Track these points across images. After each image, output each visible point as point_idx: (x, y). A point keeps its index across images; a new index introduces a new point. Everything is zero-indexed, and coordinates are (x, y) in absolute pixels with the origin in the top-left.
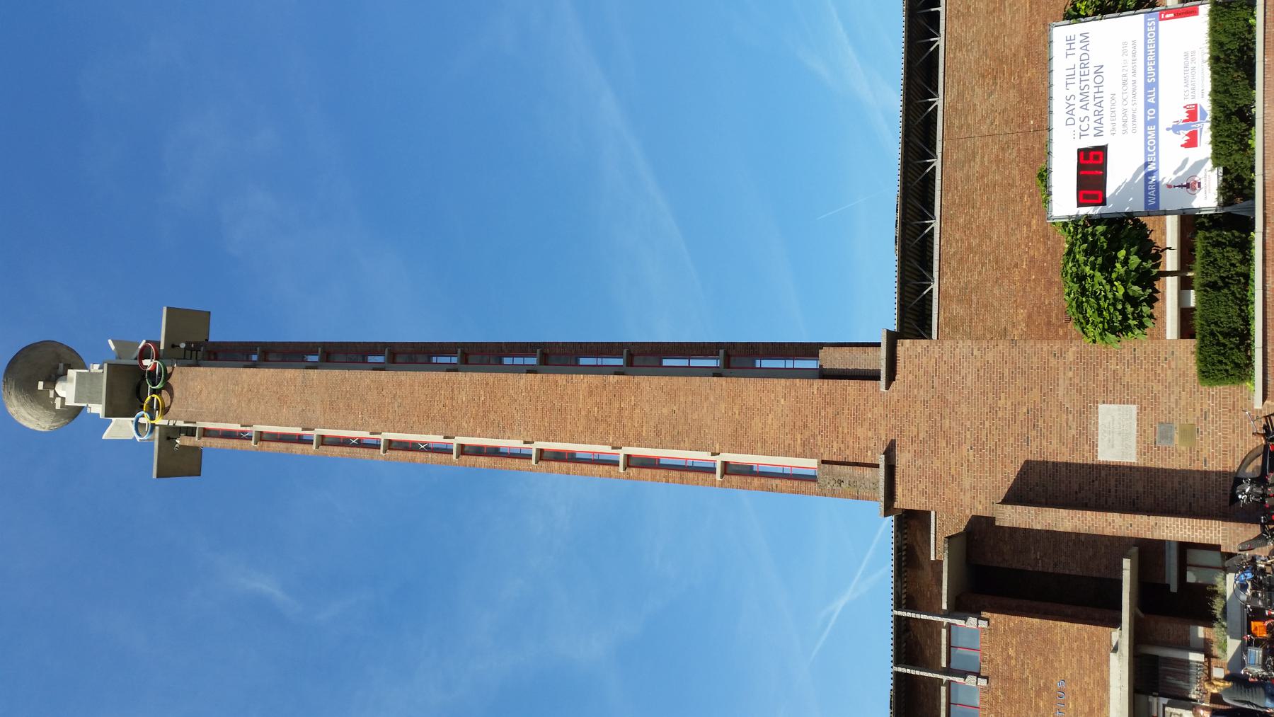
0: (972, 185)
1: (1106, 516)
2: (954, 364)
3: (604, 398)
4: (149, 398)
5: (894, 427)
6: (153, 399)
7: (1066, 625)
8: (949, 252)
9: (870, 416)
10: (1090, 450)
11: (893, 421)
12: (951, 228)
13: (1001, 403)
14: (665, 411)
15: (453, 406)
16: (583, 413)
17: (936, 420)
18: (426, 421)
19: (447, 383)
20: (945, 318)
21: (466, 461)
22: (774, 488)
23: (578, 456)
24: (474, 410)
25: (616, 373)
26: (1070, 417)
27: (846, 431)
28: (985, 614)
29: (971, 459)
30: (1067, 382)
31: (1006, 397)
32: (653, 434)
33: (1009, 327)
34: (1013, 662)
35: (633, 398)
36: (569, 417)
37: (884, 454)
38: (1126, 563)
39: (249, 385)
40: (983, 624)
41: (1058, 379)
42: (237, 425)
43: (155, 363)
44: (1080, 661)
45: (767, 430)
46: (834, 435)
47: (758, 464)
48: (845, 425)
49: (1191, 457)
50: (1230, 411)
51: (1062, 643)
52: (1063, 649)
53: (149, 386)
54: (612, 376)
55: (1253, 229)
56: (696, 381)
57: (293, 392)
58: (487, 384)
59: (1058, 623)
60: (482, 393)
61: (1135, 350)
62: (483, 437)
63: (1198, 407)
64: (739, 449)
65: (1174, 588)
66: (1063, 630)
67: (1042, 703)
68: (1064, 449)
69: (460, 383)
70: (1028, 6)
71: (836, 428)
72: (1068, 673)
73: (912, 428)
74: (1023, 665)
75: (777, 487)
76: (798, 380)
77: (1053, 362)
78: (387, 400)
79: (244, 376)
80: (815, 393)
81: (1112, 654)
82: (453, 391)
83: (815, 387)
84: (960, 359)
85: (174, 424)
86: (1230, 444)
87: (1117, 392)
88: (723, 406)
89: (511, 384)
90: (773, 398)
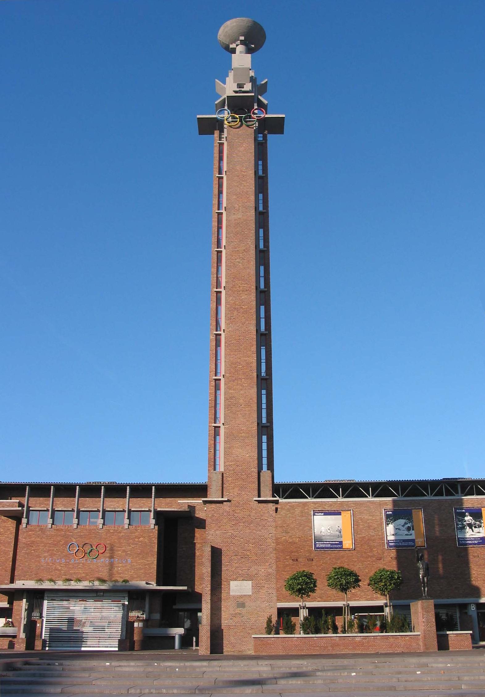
0: (358, 515)
1: (209, 585)
2: (266, 527)
3: (246, 371)
4: (237, 116)
5: (239, 503)
6: (237, 119)
7: (155, 562)
8: (326, 506)
9: (243, 493)
10: (234, 578)
11: (241, 503)
12: (337, 506)
13: (251, 545)
14: (241, 401)
15: (239, 291)
16: (239, 360)
17: (243, 520)
18: (232, 277)
19: (250, 287)
20: (293, 505)
21: (213, 296)
22: (210, 451)
23: (218, 392)
24: (238, 303)
25: (257, 375)
26: (246, 571)
27: (236, 483)
28: (157, 527)
29: (228, 534)
30: (260, 569)
31: (253, 547)
32: (231, 396)
33: (290, 534)
34: (136, 540)
35: (246, 385)
36: (237, 353)
37: (228, 499)
38: (185, 588)
39: (246, 175)
40: (152, 526)
41: (261, 566)
42: (225, 284)
43: (255, 119)
44: (140, 569)
45: (235, 449)
46: (234, 479)
47: (221, 349)
48: (239, 483)
49: (233, 614)
50: (251, 627)
51: (147, 561)
52: (145, 561)
53: (244, 116)
54: (256, 374)
55: (25, 625)
56: (255, 415)
57: (243, 201)
58: (251, 309)
59: (156, 559)
60: (246, 307)
61: (273, 594)
62: (225, 309)
63: (251, 616)
64: (227, 437)
65: (174, 607)
66: (153, 561)
67: (120, 552)
68: (234, 569)
69: (250, 295)
70: (443, 538)
71: (237, 479)
72: (135, 564)
73: (239, 511)
74: (136, 544)
75: (211, 451)
76: (257, 462)
77: (267, 564)
78: (241, 255)
79: (250, 172)
80: (252, 470)
81: (145, 582)
82: (247, 291)
83: (254, 470)
84: (268, 529)
85: (225, 128)
86: (238, 627)
87: (257, 588)
88: (245, 428)
89: (251, 322)
90: (249, 451)
